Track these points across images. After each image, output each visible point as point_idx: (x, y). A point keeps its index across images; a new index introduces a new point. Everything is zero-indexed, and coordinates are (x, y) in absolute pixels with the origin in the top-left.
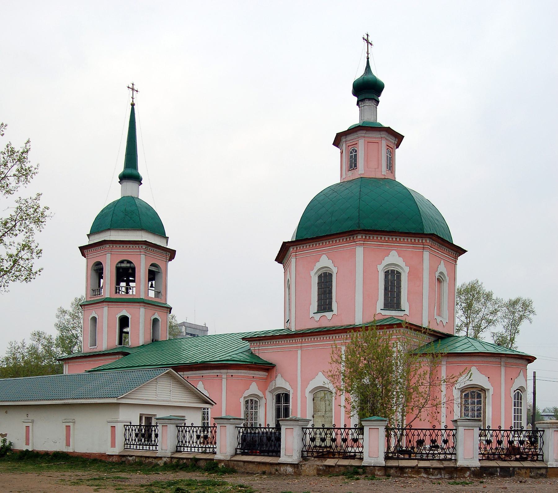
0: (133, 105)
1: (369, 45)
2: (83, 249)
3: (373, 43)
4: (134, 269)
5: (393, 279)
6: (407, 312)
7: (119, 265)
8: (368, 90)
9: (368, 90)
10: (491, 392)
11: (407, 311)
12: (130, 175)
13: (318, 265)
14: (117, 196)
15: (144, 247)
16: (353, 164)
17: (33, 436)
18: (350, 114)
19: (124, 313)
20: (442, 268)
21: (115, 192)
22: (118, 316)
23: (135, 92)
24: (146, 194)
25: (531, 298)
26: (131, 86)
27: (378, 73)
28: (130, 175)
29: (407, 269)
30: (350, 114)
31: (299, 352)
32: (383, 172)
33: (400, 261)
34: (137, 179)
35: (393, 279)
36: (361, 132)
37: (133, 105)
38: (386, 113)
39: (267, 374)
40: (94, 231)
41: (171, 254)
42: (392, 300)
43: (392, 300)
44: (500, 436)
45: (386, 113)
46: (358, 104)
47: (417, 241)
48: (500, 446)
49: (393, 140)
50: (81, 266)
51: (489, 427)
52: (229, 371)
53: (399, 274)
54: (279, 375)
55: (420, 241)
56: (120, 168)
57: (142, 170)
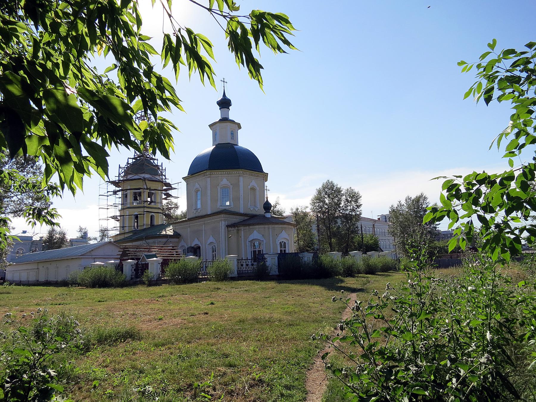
18: (216, 115)
26: (223, 80)
27: (228, 96)
38: (233, 114)
45: (233, 114)
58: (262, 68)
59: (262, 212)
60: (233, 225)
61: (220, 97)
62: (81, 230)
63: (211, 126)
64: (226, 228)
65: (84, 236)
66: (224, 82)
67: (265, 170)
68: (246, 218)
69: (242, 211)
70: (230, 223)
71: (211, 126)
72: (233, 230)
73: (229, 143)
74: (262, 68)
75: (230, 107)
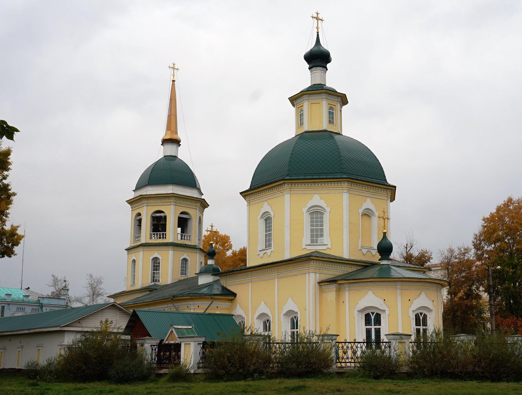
0: (318, 33)
2: (131, 202)
3: (323, 19)
4: (165, 217)
6: (329, 246)
7: (154, 215)
8: (318, 58)
9: (318, 58)
10: (387, 313)
13: (263, 211)
14: (160, 155)
16: (300, 117)
18: (304, 77)
19: (156, 255)
21: (157, 153)
23: (175, 71)
24: (183, 154)
25: (227, 234)
26: (315, 15)
27: (325, 45)
30: (304, 77)
31: (250, 284)
32: (324, 125)
34: (177, 142)
36: (305, 96)
37: (318, 33)
38: (334, 77)
39: (230, 304)
40: (138, 188)
41: (204, 205)
43: (316, 234)
45: (334, 77)
46: (309, 69)
50: (127, 214)
52: (196, 303)
54: (238, 305)
56: (162, 133)
57: (181, 135)
58: (17, 131)
59: (376, 257)
60: (332, 281)
61: (309, 46)
62: (56, 281)
63: (293, 100)
64: (317, 285)
65: (61, 292)
66: (317, 19)
67: (390, 181)
68: (353, 269)
69: (346, 255)
70: (325, 277)
71: (293, 100)
72: (331, 293)
73: (325, 131)
74: (17, 131)
75: (328, 66)
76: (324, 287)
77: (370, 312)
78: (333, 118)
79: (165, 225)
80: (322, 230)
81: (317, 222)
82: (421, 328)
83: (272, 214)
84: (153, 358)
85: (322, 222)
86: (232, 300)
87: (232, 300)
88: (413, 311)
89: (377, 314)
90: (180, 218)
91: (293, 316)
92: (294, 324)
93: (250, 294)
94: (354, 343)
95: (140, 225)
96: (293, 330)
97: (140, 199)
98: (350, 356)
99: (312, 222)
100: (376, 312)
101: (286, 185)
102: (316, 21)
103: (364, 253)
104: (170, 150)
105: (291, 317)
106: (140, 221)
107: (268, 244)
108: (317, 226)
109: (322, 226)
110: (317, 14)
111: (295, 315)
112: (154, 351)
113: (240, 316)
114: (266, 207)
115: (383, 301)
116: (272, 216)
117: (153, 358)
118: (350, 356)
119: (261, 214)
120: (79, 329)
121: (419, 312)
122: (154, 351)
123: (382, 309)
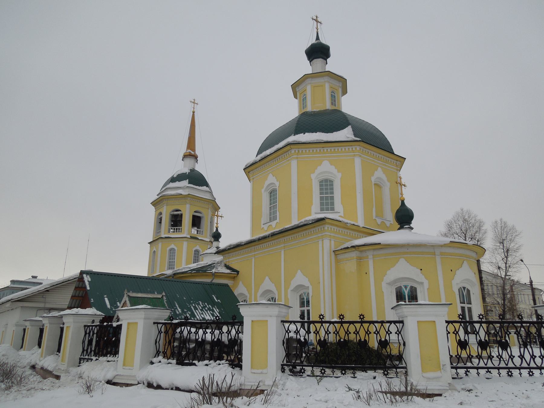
0: (194, 112)
1: (319, 24)
4: (182, 215)
5: (326, 186)
7: (172, 213)
8: (318, 52)
11: (338, 213)
12: (191, 155)
13: (267, 183)
15: (189, 199)
17: (64, 344)
20: (379, 174)
22: (168, 249)
27: (324, 40)
28: (191, 155)
29: (339, 175)
30: (306, 67)
32: (328, 106)
33: (332, 169)
34: (195, 157)
35: (326, 186)
36: (308, 80)
37: (194, 112)
42: (327, 203)
43: (327, 203)
44: (383, 333)
47: (347, 150)
48: (464, 352)
49: (338, 85)
51: (321, 316)
53: (331, 181)
54: (241, 283)
55: (351, 149)
56: (183, 149)
57: (198, 151)
64: (333, 254)
66: (317, 21)
76: (340, 257)
77: (402, 284)
78: (335, 101)
79: (181, 221)
80: (332, 198)
81: (326, 189)
82: (466, 306)
83: (277, 184)
84: (86, 348)
85: (332, 189)
86: (234, 278)
87: (234, 278)
88: (457, 284)
89: (412, 287)
90: (194, 217)
91: (302, 292)
92: (304, 302)
93: (253, 270)
94: (362, 322)
95: (160, 223)
96: (303, 309)
97: (161, 200)
98: (474, 354)
99: (321, 189)
100: (410, 284)
101: (293, 151)
102: (315, 23)
103: (379, 223)
104: (190, 162)
105: (299, 294)
106: (161, 219)
107: (272, 217)
108: (327, 193)
109: (332, 193)
110: (317, 17)
111: (304, 291)
112: (87, 335)
113: (242, 294)
114: (271, 179)
115: (420, 271)
116: (277, 188)
117: (86, 348)
118: (474, 354)
119: (265, 186)
120: (41, 305)
121: (462, 285)
122: (87, 335)
123: (420, 281)
